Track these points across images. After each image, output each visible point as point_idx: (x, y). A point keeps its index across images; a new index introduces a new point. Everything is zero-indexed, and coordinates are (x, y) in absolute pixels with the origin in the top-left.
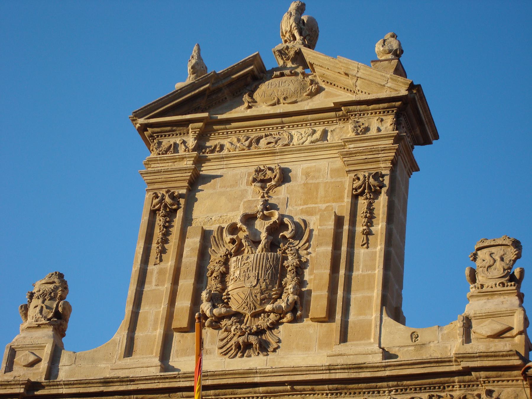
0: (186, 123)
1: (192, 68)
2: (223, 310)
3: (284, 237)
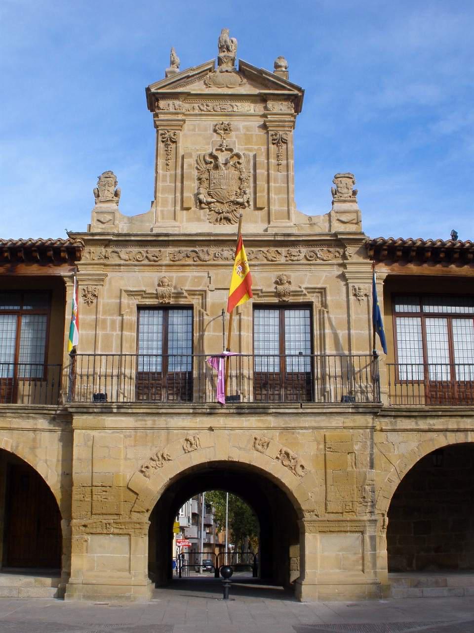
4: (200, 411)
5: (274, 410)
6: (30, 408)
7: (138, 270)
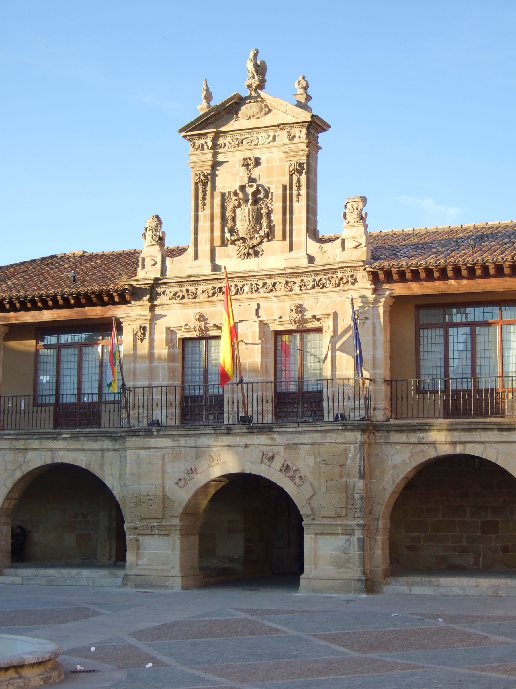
0: (206, 134)
1: (204, 97)
2: (236, 238)
3: (260, 197)
4: (219, 432)
5: (277, 430)
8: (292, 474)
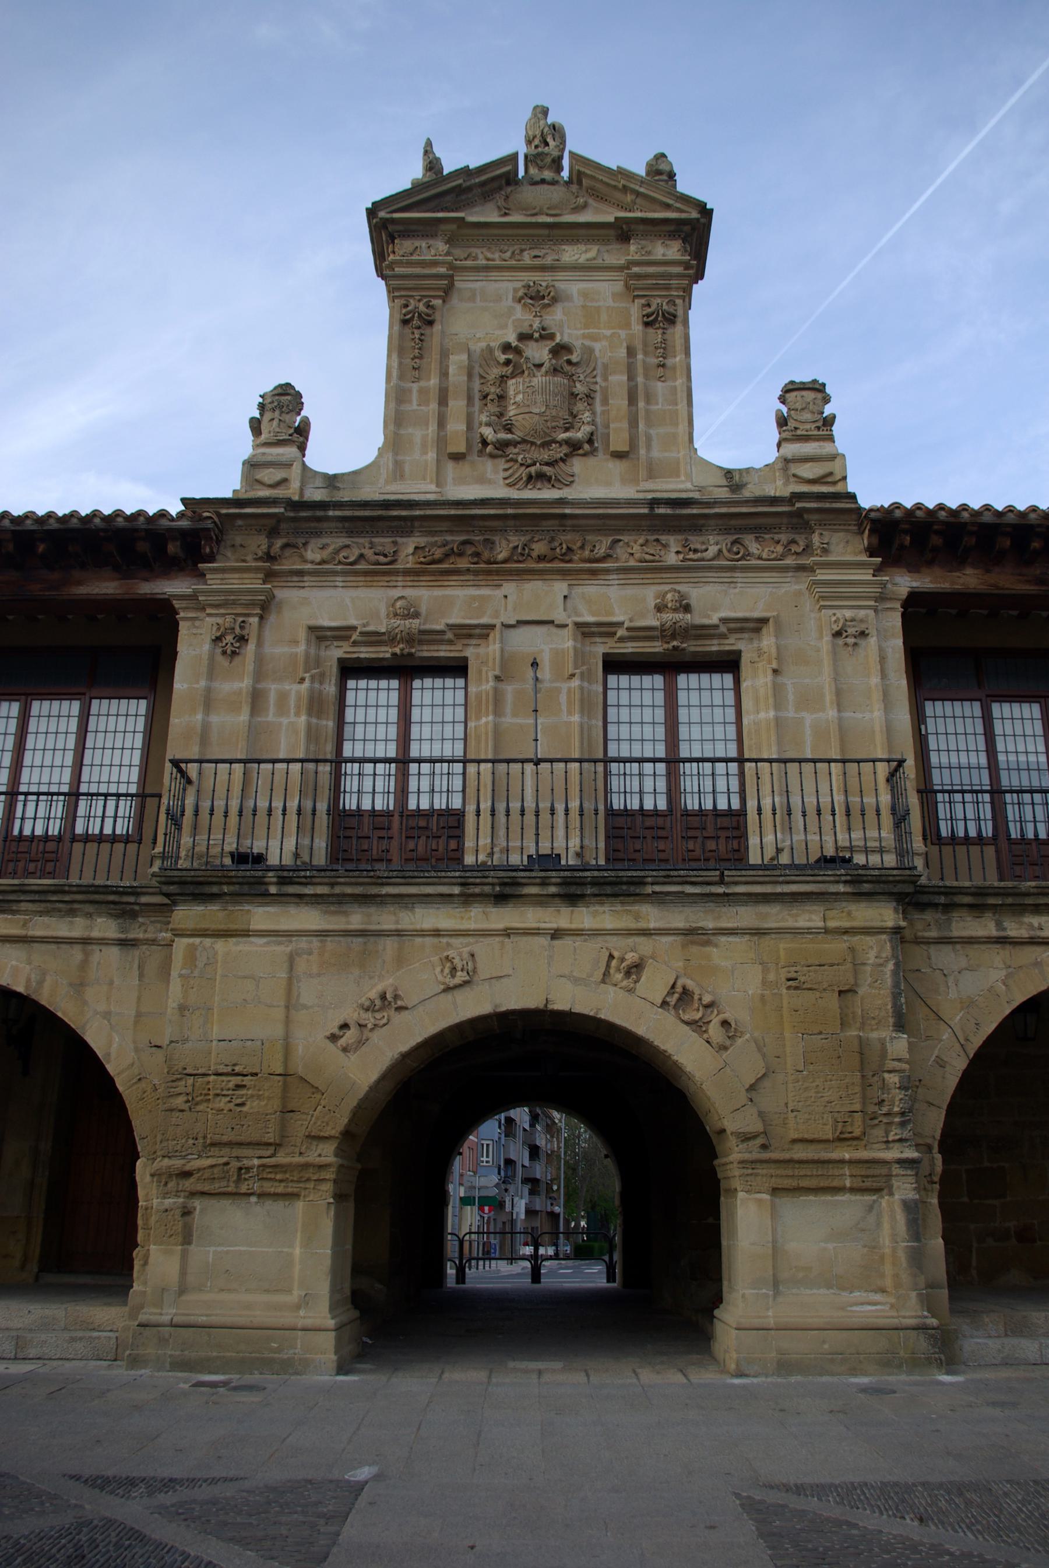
4: (477, 890)
6: (75, 889)
7: (341, 584)
8: (700, 1015)
